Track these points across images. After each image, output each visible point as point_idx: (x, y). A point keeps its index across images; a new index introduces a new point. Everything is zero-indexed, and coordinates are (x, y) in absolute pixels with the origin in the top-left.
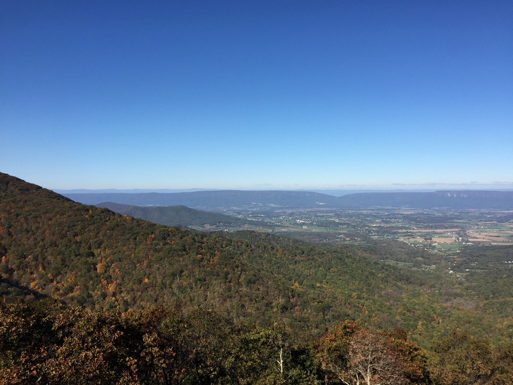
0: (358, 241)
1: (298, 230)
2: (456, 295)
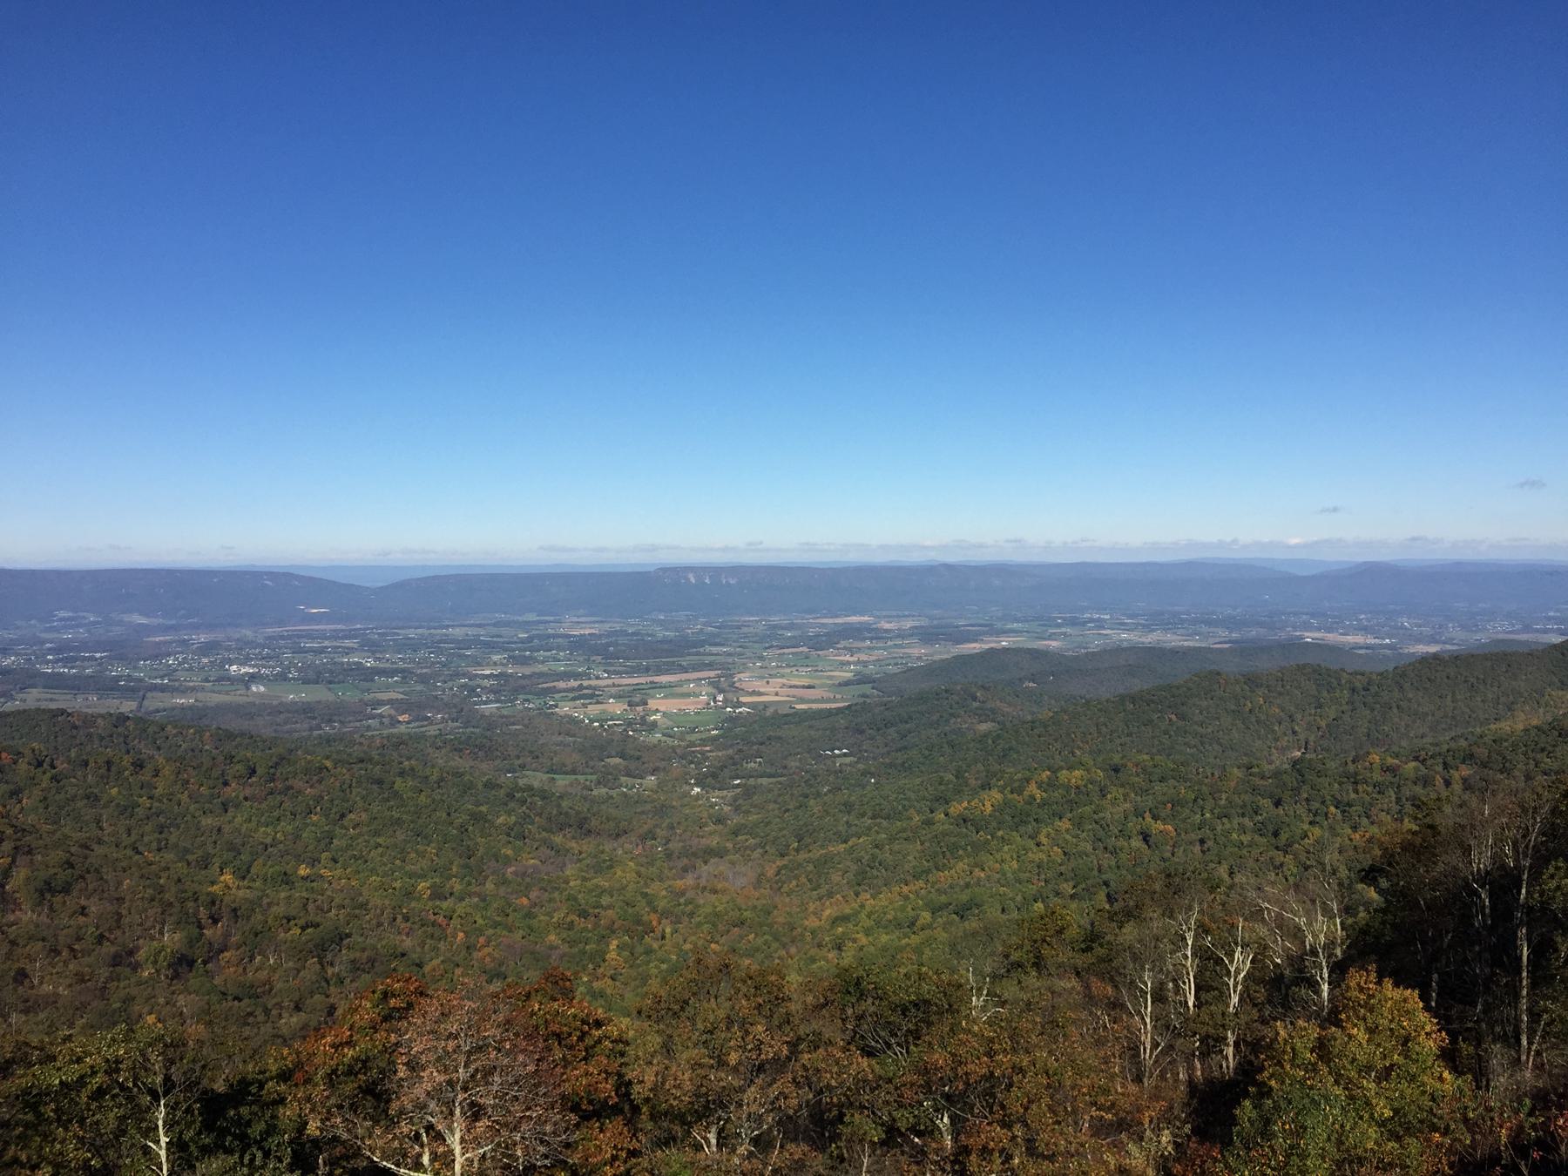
0: (438, 723)
1: (235, 697)
2: (709, 853)
